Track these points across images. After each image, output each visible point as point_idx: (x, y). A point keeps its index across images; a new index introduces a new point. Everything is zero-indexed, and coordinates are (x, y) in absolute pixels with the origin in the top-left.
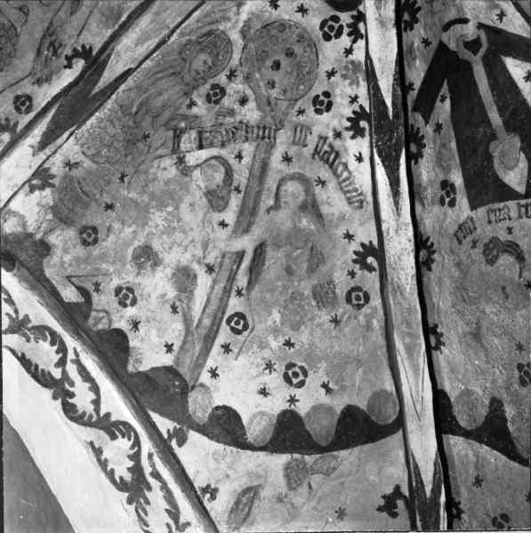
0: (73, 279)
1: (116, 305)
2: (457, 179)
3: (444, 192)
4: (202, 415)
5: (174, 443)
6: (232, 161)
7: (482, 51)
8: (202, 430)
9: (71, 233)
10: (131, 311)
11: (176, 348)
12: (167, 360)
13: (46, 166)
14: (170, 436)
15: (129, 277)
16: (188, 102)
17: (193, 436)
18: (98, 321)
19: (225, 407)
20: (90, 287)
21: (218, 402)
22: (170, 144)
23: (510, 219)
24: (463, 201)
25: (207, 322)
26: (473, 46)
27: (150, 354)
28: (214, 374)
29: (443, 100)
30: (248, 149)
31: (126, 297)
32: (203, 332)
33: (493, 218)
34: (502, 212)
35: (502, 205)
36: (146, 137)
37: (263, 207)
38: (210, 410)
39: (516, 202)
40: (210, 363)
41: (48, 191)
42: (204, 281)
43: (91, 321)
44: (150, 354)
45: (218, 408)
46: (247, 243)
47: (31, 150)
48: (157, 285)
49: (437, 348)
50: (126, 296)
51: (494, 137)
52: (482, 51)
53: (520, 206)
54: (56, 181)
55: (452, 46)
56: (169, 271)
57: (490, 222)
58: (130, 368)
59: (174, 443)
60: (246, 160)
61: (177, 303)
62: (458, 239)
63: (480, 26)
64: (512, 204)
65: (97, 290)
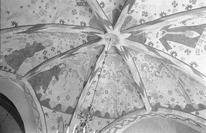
0: (165, 104)
1: (173, 102)
2: (186, 48)
3: (187, 53)
4: (197, 108)
5: (198, 115)
6: (164, 71)
7: (165, 31)
8: (199, 110)
9: (159, 98)
10: (175, 101)
11: (185, 101)
12: (186, 104)
13: (148, 96)
14: (196, 114)
15: (171, 97)
16: (151, 72)
17: (199, 112)
18: (173, 106)
19: (199, 104)
20: (168, 103)
21: (197, 104)
22: (156, 77)
23: (203, 40)
24: (190, 49)
25: (185, 94)
26: (164, 32)
27: (183, 105)
28: (193, 101)
29: (170, 43)
30: (163, 68)
31: (173, 100)
32: (186, 95)
33: (200, 44)
34: (201, 41)
35: (199, 41)
36: (153, 80)
37: (174, 73)
38: (198, 106)
39: (187, 26)
40: (191, 100)
41: (151, 97)
42: (179, 88)
43: (172, 107)
44: (183, 105)
45: (198, 105)
46: (178, 79)
47: (144, 98)
48: (175, 95)
49: (165, 14)
50: (173, 100)
51: (184, 35)
52: (165, 31)
53: (202, 37)
54: (151, 96)
55: (161, 37)
56: (174, 91)
57: (200, 45)
58: (183, 109)
59: (198, 115)
60: (165, 69)
61: (179, 94)
62: (198, 55)
63: (160, 30)
64: (200, 38)
65: (169, 102)
